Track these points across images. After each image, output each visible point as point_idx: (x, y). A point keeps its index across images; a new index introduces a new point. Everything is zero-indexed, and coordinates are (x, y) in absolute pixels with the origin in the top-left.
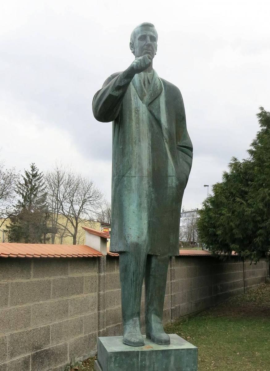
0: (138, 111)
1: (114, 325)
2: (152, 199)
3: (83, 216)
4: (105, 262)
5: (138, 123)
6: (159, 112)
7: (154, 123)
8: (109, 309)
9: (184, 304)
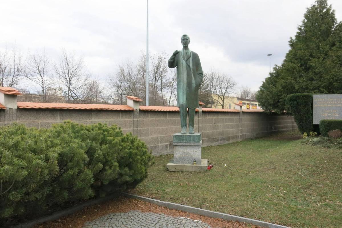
0: (183, 63)
1: (207, 138)
2: (187, 91)
3: (227, 95)
4: (201, 114)
5: (183, 67)
6: (190, 63)
7: (188, 67)
8: (204, 132)
9: (248, 133)
